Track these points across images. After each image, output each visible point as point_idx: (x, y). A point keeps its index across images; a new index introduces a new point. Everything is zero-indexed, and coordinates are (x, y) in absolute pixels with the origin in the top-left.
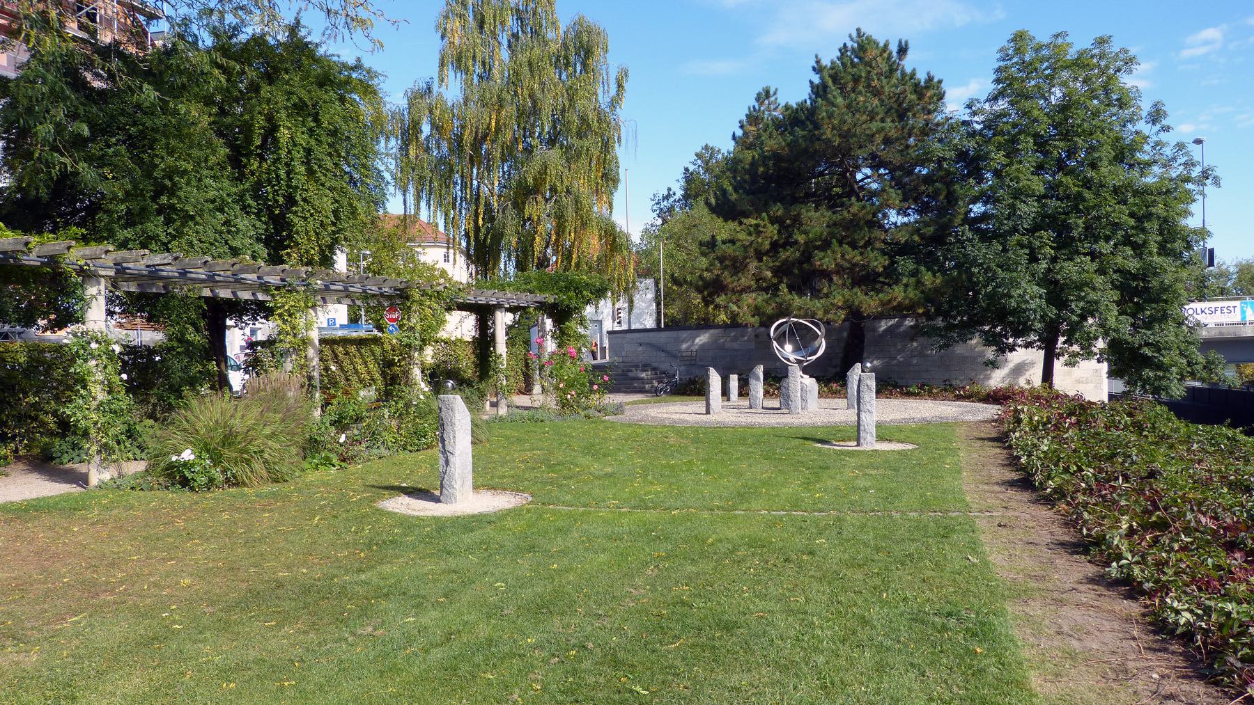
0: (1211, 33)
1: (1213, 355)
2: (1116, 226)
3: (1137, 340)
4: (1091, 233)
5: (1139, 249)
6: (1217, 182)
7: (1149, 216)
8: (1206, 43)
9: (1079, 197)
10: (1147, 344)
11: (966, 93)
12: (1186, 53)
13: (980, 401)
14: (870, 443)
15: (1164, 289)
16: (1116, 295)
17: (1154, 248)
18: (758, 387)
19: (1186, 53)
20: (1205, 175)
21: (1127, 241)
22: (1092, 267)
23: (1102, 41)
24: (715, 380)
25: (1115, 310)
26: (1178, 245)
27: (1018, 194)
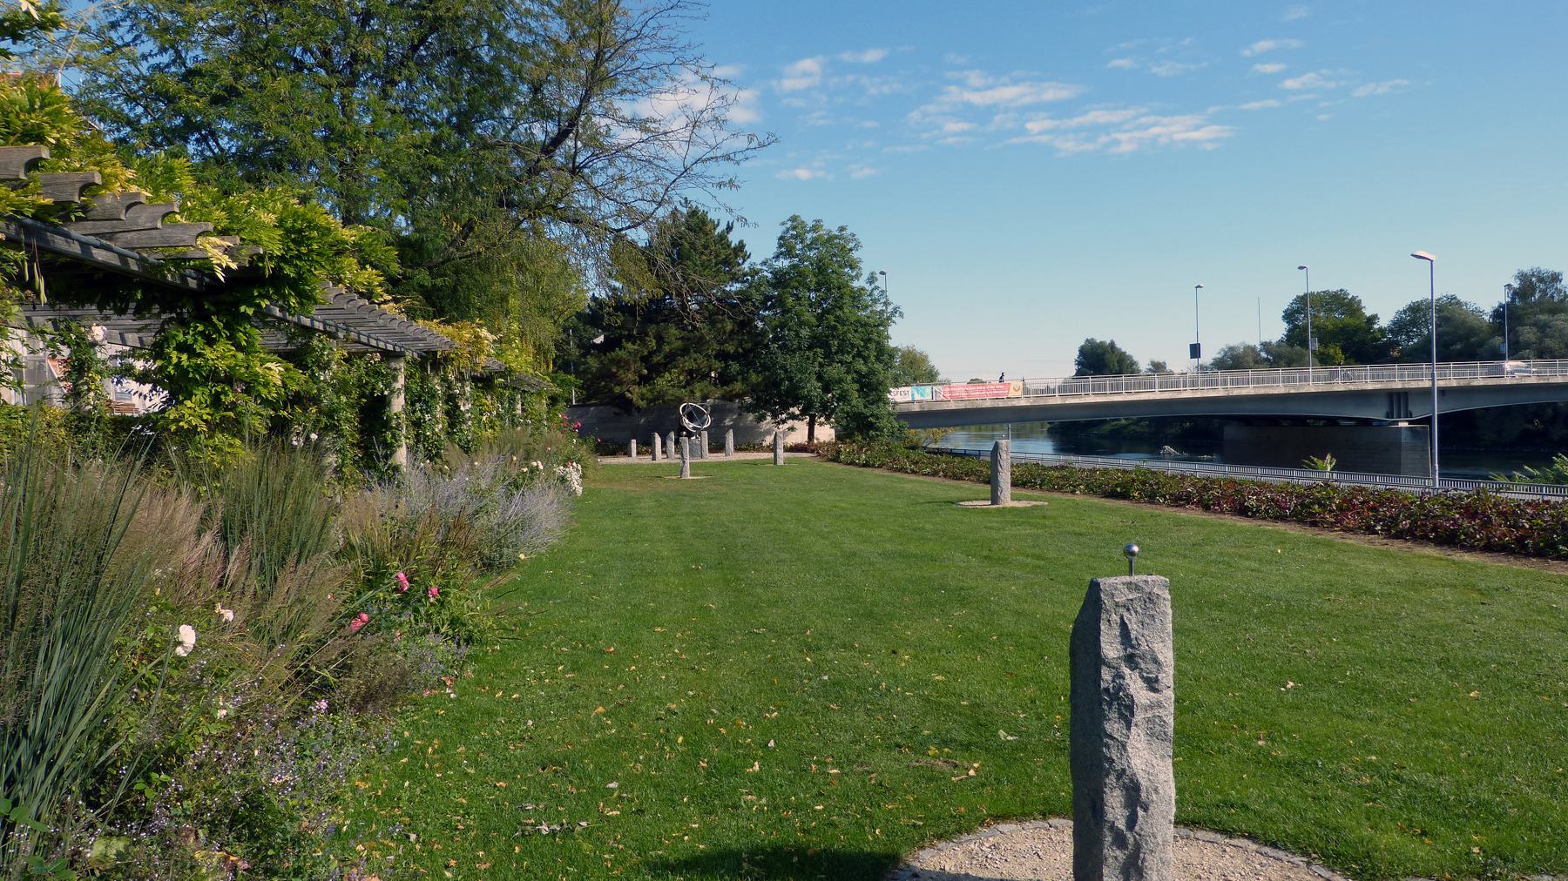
0: (808, 64)
1: (902, 422)
2: (853, 346)
3: (867, 412)
4: (841, 350)
5: (866, 359)
6: (901, 315)
7: (870, 340)
8: (805, 74)
9: (835, 328)
10: (32, 53)
11: (761, 250)
12: (788, 84)
13: (1394, 532)
14: (688, 476)
15: (880, 384)
16: (856, 386)
17: (873, 359)
18: (671, 446)
19: (788, 84)
20: (895, 310)
21: (859, 354)
22: (843, 369)
23: (842, 229)
24: (658, 440)
25: (856, 394)
26: (885, 357)
27: (801, 324)
